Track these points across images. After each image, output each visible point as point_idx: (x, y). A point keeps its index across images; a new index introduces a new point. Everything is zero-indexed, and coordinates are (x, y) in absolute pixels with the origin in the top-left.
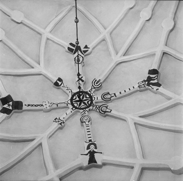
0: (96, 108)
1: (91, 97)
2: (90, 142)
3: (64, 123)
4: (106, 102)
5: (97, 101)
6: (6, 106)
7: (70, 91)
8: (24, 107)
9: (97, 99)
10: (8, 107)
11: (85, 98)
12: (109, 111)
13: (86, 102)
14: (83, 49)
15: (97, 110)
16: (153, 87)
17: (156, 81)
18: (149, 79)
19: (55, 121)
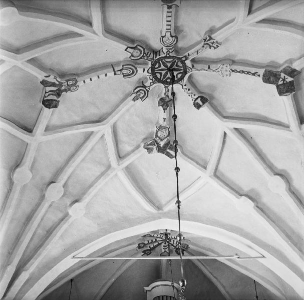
0: (148, 55)
1: (153, 73)
2: (170, 4)
3: (204, 39)
5: (144, 66)
6: (289, 79)
7: (184, 87)
8: (261, 72)
9: (144, 70)
10: (286, 77)
11: (163, 72)
12: (129, 49)
13: (163, 67)
14: (155, 148)
15: (148, 52)
16: (54, 81)
17: (48, 89)
18: (58, 94)
19: (219, 45)
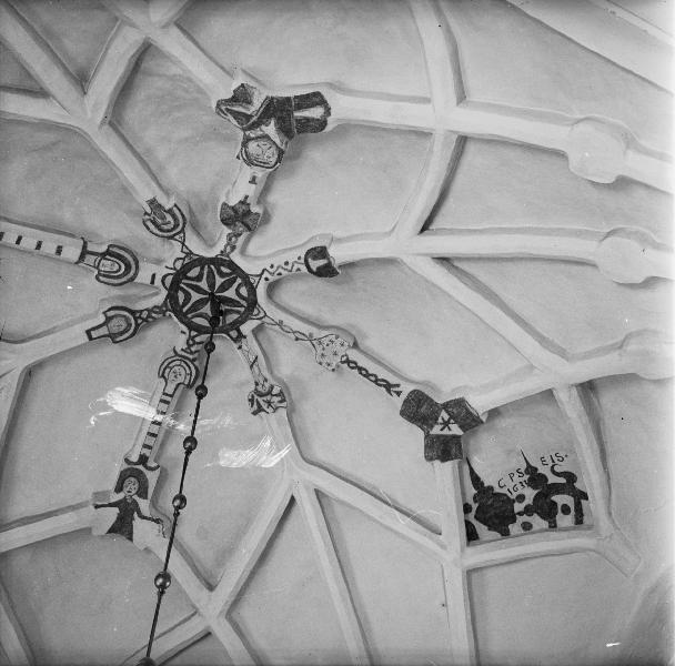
4: (122, 253)
10: (446, 432)
11: (204, 284)
